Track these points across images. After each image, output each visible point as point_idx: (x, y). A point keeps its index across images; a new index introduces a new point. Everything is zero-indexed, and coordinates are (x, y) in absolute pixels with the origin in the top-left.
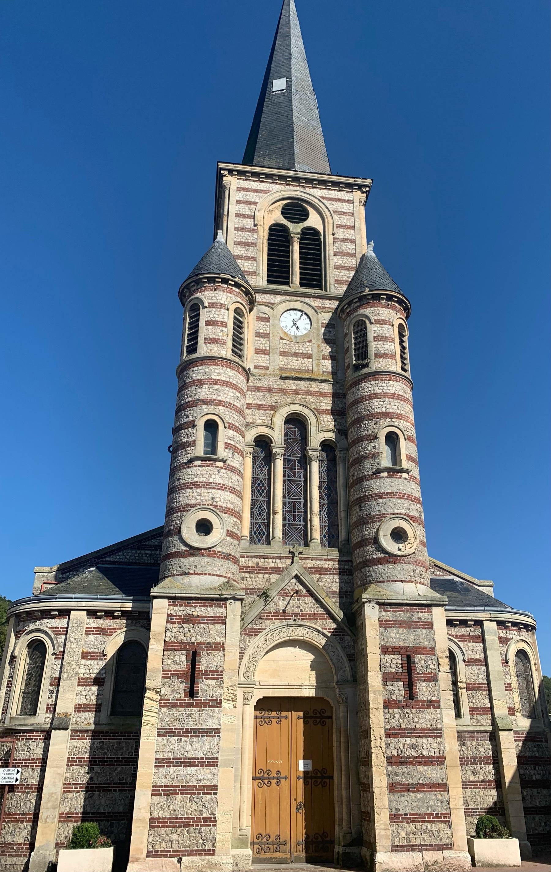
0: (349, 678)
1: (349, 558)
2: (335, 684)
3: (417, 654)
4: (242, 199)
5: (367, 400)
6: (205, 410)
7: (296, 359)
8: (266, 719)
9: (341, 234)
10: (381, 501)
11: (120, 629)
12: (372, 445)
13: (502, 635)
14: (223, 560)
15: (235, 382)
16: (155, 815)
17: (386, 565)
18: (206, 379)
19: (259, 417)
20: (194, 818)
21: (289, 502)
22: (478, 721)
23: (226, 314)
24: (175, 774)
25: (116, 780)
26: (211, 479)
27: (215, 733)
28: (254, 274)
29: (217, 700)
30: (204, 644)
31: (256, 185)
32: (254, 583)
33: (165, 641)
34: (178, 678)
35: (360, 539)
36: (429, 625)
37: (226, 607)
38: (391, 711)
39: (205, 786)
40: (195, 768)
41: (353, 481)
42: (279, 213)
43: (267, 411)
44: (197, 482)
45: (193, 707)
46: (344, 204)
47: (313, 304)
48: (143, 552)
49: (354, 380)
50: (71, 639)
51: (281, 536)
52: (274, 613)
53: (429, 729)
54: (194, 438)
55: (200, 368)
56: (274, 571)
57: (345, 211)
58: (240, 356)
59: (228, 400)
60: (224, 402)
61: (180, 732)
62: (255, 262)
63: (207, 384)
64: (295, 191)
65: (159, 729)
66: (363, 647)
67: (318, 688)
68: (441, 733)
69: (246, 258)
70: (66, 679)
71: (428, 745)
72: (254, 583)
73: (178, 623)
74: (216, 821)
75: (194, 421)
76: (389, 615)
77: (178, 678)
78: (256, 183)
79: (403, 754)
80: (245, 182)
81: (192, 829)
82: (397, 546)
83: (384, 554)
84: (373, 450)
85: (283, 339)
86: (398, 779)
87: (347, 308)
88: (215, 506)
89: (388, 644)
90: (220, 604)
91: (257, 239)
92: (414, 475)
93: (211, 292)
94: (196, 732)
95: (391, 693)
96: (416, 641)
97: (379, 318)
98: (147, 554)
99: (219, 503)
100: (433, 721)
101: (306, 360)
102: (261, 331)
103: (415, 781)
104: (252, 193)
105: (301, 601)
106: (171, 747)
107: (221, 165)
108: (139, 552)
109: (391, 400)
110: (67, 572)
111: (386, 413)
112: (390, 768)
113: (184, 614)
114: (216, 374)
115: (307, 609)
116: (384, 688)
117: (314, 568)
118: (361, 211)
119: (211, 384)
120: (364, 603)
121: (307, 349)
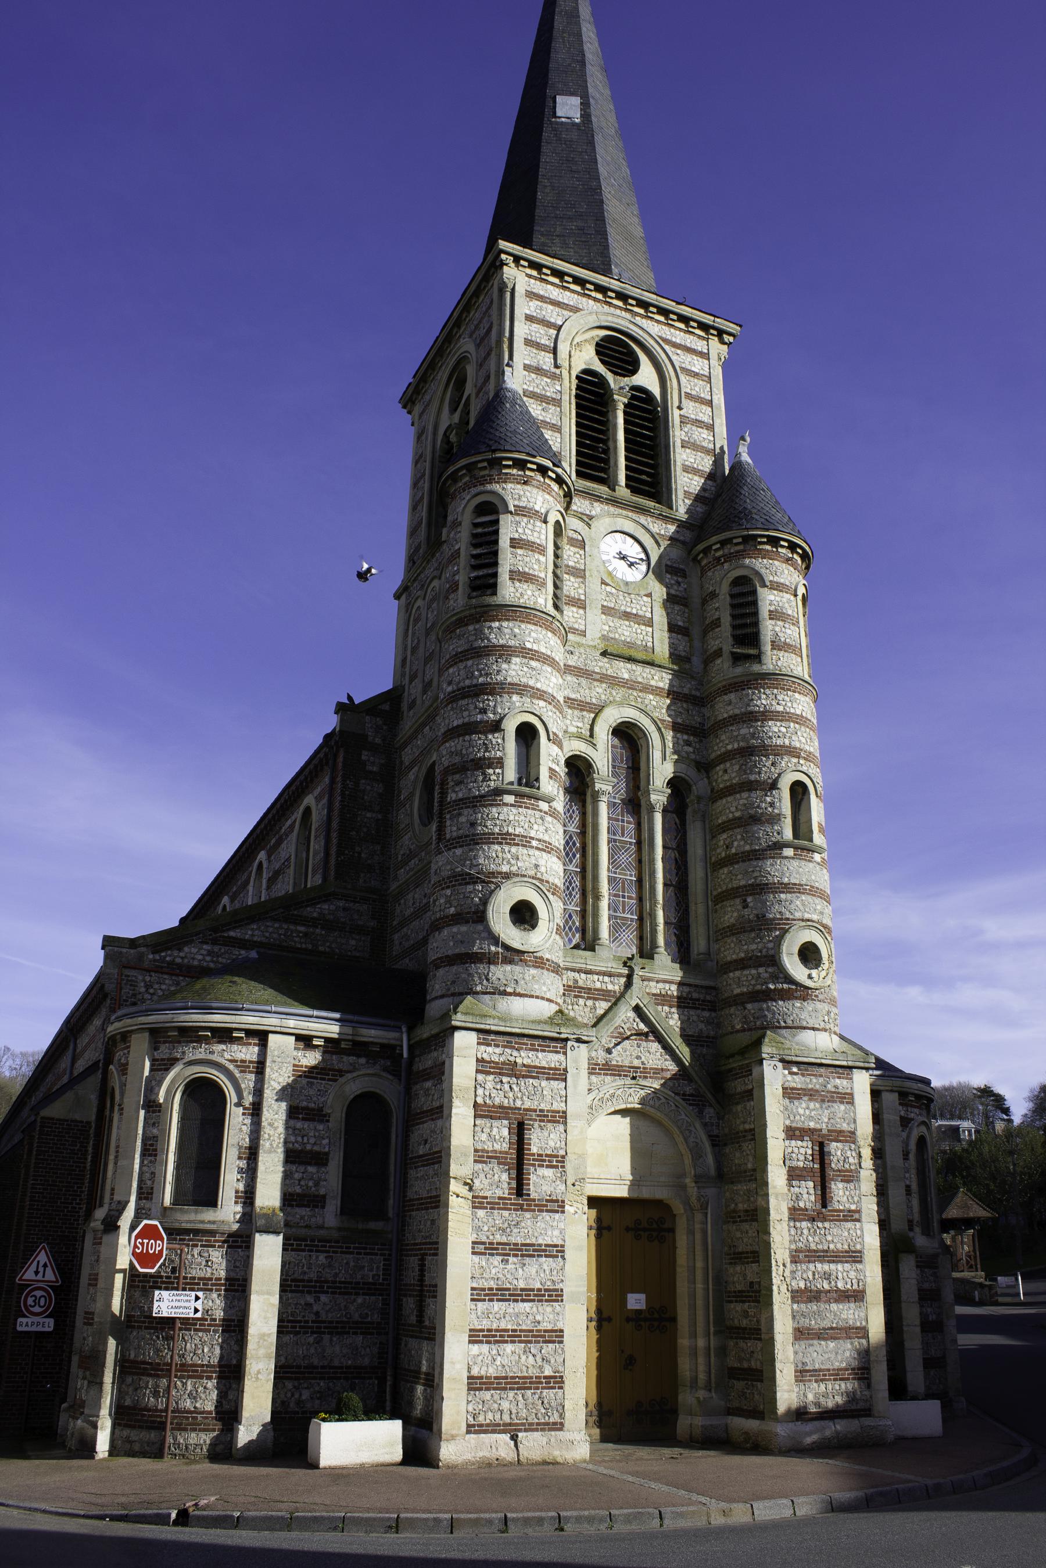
0: (713, 1172)
1: (712, 984)
3: (832, 1141)
6: (518, 704)
7: (627, 623)
9: (691, 409)
10: (783, 896)
12: (768, 799)
16: (475, 1372)
17: (791, 1002)
20: (531, 1378)
24: (502, 1312)
25: (356, 1317)
27: (557, 1251)
29: (557, 1201)
30: (535, 1111)
31: (555, 294)
33: (475, 1101)
35: (742, 955)
36: (848, 1098)
37: (565, 1053)
38: (798, 1224)
39: (545, 1331)
41: (726, 857)
43: (585, 713)
44: (511, 834)
45: (522, 1210)
47: (651, 527)
48: (292, 927)
50: (272, 1083)
54: (499, 754)
55: (505, 624)
61: (505, 1249)
64: (619, 318)
65: (474, 1243)
67: (634, 1185)
70: (270, 1152)
74: (563, 1382)
77: (499, 1163)
80: (538, 283)
81: (529, 1392)
82: (807, 972)
84: (770, 809)
85: (607, 584)
86: (805, 1322)
87: (717, 550)
89: (794, 1125)
93: (519, 486)
97: (776, 579)
98: (301, 932)
101: (643, 627)
103: (826, 1324)
104: (551, 307)
106: (494, 1271)
109: (797, 726)
110: (162, 951)
112: (795, 1306)
117: (660, 995)
121: (644, 609)
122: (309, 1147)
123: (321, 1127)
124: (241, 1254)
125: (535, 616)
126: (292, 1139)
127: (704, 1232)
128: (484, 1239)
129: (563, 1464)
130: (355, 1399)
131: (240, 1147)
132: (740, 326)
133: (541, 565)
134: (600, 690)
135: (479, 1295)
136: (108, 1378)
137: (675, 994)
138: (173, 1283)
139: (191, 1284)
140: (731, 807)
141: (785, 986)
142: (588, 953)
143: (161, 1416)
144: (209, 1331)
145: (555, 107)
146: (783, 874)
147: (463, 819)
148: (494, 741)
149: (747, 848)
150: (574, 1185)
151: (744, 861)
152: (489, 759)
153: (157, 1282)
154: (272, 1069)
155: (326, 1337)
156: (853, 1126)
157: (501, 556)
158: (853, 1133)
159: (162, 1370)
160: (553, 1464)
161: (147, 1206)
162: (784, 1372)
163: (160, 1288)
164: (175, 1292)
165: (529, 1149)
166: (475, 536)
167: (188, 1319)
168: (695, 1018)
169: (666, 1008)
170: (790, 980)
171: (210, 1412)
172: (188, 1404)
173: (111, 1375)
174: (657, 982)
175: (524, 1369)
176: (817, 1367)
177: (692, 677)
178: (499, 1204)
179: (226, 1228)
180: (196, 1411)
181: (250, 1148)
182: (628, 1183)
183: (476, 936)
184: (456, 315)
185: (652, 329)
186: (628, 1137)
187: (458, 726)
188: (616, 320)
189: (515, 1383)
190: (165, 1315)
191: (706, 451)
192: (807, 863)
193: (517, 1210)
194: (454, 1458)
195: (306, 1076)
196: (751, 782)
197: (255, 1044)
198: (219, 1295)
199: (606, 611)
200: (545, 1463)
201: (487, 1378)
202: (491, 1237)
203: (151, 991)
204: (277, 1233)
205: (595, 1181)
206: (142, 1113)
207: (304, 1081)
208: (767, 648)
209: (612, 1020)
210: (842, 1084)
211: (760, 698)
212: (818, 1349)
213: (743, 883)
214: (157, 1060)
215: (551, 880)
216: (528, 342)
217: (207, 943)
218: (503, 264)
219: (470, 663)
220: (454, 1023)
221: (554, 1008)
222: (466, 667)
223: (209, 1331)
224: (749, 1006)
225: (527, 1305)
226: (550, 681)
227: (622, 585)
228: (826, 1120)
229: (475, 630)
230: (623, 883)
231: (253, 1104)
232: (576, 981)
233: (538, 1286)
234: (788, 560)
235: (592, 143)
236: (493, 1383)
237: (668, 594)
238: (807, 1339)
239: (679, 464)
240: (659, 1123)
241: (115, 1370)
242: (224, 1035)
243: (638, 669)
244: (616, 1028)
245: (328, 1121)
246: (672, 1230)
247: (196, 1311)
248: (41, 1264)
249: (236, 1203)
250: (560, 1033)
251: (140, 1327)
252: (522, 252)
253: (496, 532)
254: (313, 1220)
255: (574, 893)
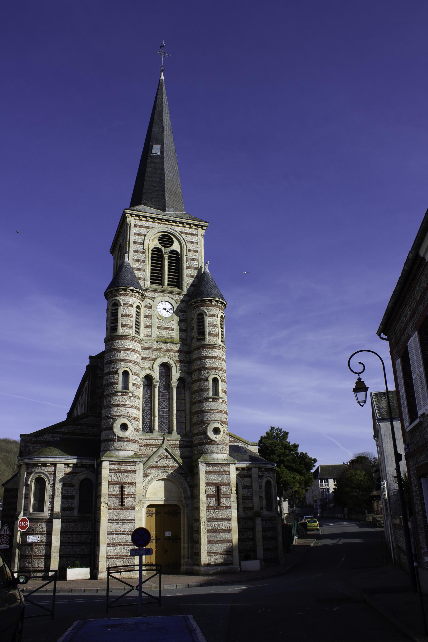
0: (190, 496)
1: (191, 440)
2: (183, 498)
3: (222, 486)
4: (137, 232)
5: (203, 359)
6: (123, 365)
7: (165, 331)
8: (150, 514)
9: (190, 255)
11: (81, 473)
12: (205, 384)
13: (260, 474)
14: (133, 443)
15: (136, 349)
16: (109, 554)
17: (210, 446)
18: (123, 348)
19: (147, 364)
20: (125, 555)
21: (161, 410)
22: (246, 513)
23: (132, 310)
24: (116, 538)
26: (126, 403)
27: (133, 521)
28: (144, 279)
29: (133, 507)
30: (127, 482)
31: (145, 224)
32: (145, 452)
33: (109, 481)
34: (116, 497)
35: (197, 432)
36: (228, 473)
37: (136, 466)
39: (129, 543)
40: (125, 536)
42: (156, 241)
43: (151, 361)
44: (120, 404)
45: (123, 510)
46: (193, 236)
48: (76, 427)
49: (196, 347)
50: (58, 477)
51: (157, 429)
52: (155, 466)
53: (226, 518)
55: (119, 341)
56: (154, 446)
57: (193, 241)
58: (140, 336)
59: (133, 359)
60: (132, 360)
61: (118, 521)
62: (144, 272)
63: (123, 351)
64: (166, 228)
65: (108, 519)
66: (197, 483)
67: (165, 500)
68: (231, 519)
69: (139, 270)
70: (58, 496)
71: (225, 525)
72: (145, 452)
73: (114, 473)
75: (117, 371)
76: (210, 469)
78: (145, 222)
79: (214, 529)
82: (215, 436)
83: (209, 440)
84: (205, 387)
85: (159, 319)
87: (194, 304)
88: (129, 416)
89: (209, 482)
90: (133, 464)
91: (145, 258)
92: (225, 400)
93: (124, 297)
94: (125, 521)
95: (210, 503)
96: (222, 480)
97: (211, 313)
98: (79, 428)
99: (131, 415)
100: (228, 515)
101: (171, 331)
102: (147, 314)
103: (218, 539)
104: (143, 229)
105: (167, 461)
106: (114, 527)
107: (126, 211)
108: (74, 427)
109: (215, 360)
110: (37, 437)
111: (213, 367)
112: (208, 534)
113: (117, 468)
114: (127, 345)
115: (170, 464)
116: (207, 501)
117: (174, 444)
118: (202, 241)
119: (125, 351)
120: (199, 463)
121: (171, 325)
122: (69, 494)
123: (72, 489)
124: (50, 525)
125: (129, 337)
126: (64, 492)
127: (187, 513)
128: (111, 518)
129: (134, 579)
130: (78, 562)
131: (50, 495)
132: (209, 223)
133: (132, 321)
134: (156, 353)
135: (110, 534)
136: (16, 560)
137: (179, 444)
138: (32, 533)
139: (37, 534)
140: (195, 387)
141: (208, 441)
142: (151, 434)
143: (30, 569)
144: (42, 546)
145: (152, 150)
146: (209, 407)
147: (108, 400)
148: (116, 377)
149: (199, 399)
150: (138, 502)
151: (198, 403)
152: (114, 382)
153: (28, 533)
154: (58, 473)
155: (75, 546)
156: (229, 481)
157: (119, 320)
158: (229, 483)
159: (30, 557)
160: (131, 579)
161: (26, 513)
162: (204, 553)
163: (29, 535)
164: (33, 536)
165: (125, 493)
166: (112, 313)
167: (36, 543)
168: (185, 451)
169: (176, 448)
170: (210, 439)
171: (42, 568)
172: (37, 566)
173: (17, 559)
174: (173, 441)
175: (123, 553)
176: (215, 551)
177: (187, 345)
178: (116, 508)
179: (46, 518)
180: (39, 567)
181: (52, 496)
182: (164, 500)
183: (110, 434)
184: (118, 229)
185: (177, 229)
186: (164, 487)
187: (107, 372)
188: (165, 229)
189: (121, 557)
190: (30, 542)
191: (196, 268)
192: (217, 403)
193: (121, 510)
194: (102, 577)
195: (68, 475)
196: (201, 379)
197: (53, 467)
198: (45, 536)
199: (159, 328)
200: (129, 578)
201: (112, 556)
202: (113, 518)
203: (34, 449)
204: (59, 519)
205: (153, 500)
206: (24, 487)
207: (68, 476)
208: (207, 336)
209: (157, 453)
210: (226, 469)
211: (204, 352)
212: (215, 546)
213: (198, 410)
214: (28, 472)
215: (133, 416)
216: (135, 242)
217: (51, 434)
218: (126, 217)
219: (110, 353)
220: (102, 459)
221: (134, 453)
222: (109, 355)
223: (42, 546)
224: (198, 447)
225: (124, 536)
226: (134, 357)
227: (164, 318)
228: (220, 480)
229: (111, 343)
230: (164, 411)
231: (53, 483)
232: (147, 443)
233: (127, 530)
234: (215, 306)
235: (163, 162)
236: (114, 557)
237: (180, 319)
238: (212, 543)
239: (185, 275)
240: (174, 482)
241: (18, 558)
242: (45, 465)
243: (169, 345)
244: (159, 455)
245: (75, 487)
246: (180, 513)
247: (38, 541)
248: (5, 530)
249: (49, 511)
250: (134, 460)
251: (25, 546)
252: (133, 212)
253: (118, 312)
254: (71, 514)
255: (148, 416)
